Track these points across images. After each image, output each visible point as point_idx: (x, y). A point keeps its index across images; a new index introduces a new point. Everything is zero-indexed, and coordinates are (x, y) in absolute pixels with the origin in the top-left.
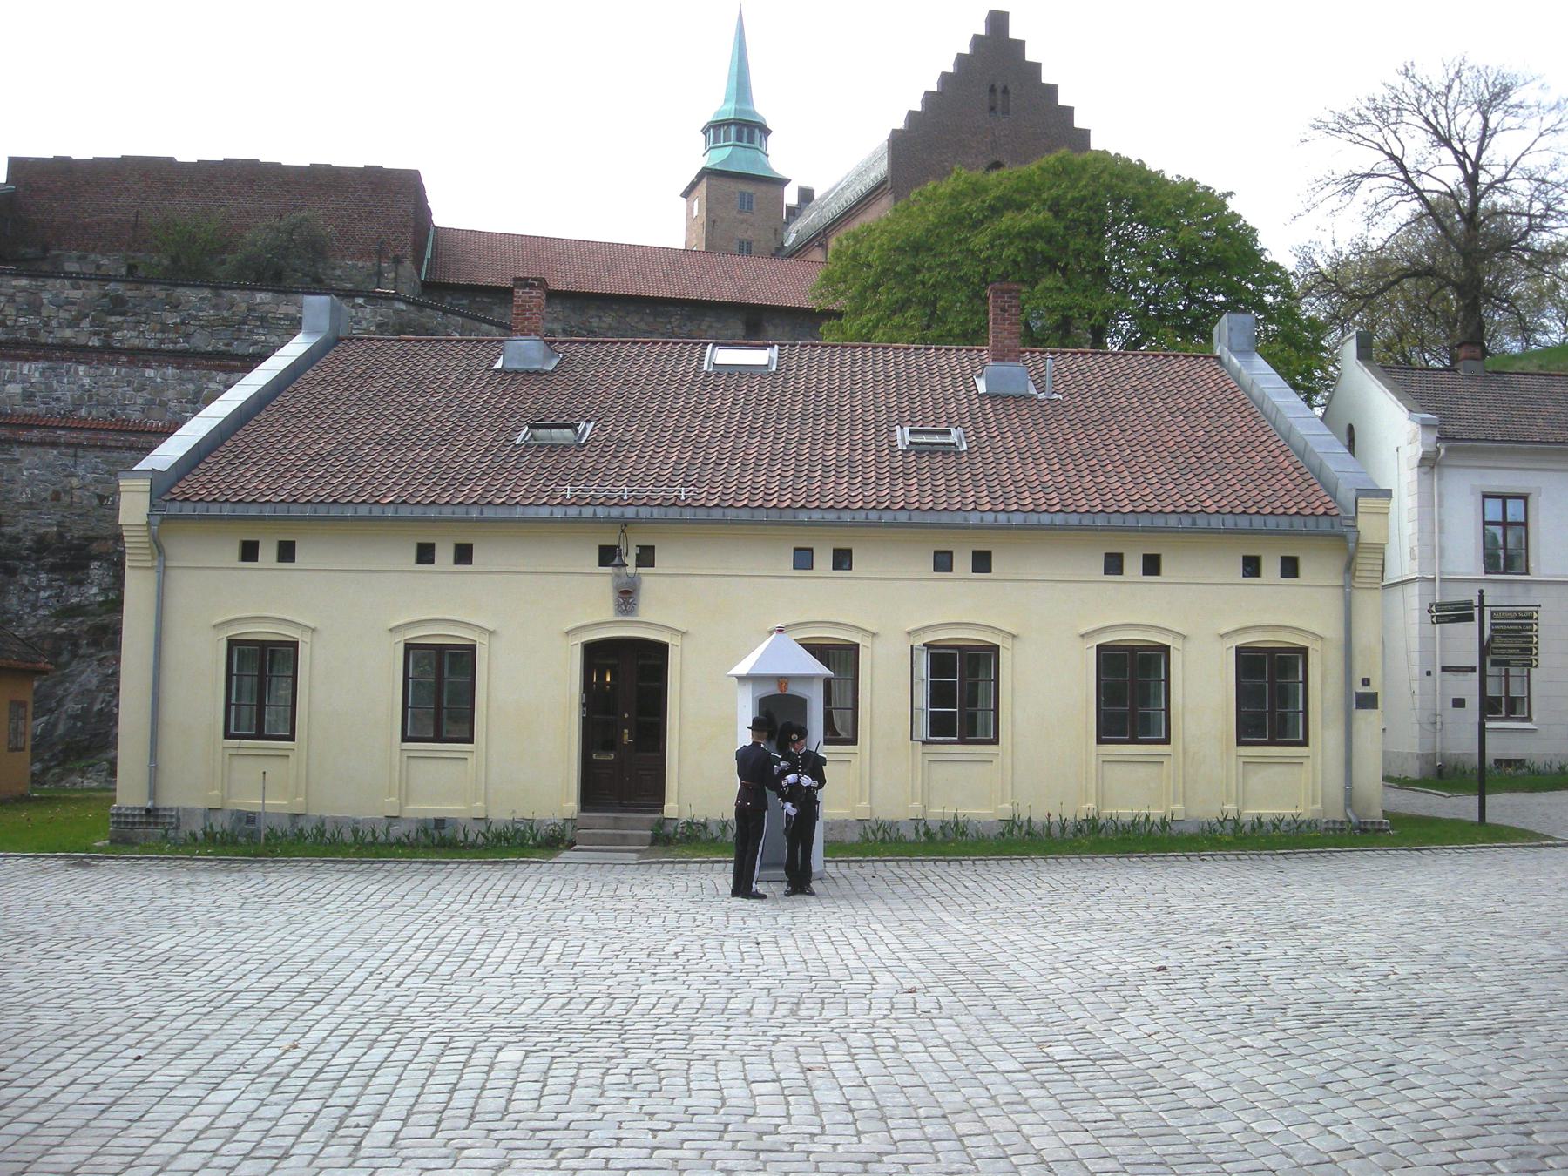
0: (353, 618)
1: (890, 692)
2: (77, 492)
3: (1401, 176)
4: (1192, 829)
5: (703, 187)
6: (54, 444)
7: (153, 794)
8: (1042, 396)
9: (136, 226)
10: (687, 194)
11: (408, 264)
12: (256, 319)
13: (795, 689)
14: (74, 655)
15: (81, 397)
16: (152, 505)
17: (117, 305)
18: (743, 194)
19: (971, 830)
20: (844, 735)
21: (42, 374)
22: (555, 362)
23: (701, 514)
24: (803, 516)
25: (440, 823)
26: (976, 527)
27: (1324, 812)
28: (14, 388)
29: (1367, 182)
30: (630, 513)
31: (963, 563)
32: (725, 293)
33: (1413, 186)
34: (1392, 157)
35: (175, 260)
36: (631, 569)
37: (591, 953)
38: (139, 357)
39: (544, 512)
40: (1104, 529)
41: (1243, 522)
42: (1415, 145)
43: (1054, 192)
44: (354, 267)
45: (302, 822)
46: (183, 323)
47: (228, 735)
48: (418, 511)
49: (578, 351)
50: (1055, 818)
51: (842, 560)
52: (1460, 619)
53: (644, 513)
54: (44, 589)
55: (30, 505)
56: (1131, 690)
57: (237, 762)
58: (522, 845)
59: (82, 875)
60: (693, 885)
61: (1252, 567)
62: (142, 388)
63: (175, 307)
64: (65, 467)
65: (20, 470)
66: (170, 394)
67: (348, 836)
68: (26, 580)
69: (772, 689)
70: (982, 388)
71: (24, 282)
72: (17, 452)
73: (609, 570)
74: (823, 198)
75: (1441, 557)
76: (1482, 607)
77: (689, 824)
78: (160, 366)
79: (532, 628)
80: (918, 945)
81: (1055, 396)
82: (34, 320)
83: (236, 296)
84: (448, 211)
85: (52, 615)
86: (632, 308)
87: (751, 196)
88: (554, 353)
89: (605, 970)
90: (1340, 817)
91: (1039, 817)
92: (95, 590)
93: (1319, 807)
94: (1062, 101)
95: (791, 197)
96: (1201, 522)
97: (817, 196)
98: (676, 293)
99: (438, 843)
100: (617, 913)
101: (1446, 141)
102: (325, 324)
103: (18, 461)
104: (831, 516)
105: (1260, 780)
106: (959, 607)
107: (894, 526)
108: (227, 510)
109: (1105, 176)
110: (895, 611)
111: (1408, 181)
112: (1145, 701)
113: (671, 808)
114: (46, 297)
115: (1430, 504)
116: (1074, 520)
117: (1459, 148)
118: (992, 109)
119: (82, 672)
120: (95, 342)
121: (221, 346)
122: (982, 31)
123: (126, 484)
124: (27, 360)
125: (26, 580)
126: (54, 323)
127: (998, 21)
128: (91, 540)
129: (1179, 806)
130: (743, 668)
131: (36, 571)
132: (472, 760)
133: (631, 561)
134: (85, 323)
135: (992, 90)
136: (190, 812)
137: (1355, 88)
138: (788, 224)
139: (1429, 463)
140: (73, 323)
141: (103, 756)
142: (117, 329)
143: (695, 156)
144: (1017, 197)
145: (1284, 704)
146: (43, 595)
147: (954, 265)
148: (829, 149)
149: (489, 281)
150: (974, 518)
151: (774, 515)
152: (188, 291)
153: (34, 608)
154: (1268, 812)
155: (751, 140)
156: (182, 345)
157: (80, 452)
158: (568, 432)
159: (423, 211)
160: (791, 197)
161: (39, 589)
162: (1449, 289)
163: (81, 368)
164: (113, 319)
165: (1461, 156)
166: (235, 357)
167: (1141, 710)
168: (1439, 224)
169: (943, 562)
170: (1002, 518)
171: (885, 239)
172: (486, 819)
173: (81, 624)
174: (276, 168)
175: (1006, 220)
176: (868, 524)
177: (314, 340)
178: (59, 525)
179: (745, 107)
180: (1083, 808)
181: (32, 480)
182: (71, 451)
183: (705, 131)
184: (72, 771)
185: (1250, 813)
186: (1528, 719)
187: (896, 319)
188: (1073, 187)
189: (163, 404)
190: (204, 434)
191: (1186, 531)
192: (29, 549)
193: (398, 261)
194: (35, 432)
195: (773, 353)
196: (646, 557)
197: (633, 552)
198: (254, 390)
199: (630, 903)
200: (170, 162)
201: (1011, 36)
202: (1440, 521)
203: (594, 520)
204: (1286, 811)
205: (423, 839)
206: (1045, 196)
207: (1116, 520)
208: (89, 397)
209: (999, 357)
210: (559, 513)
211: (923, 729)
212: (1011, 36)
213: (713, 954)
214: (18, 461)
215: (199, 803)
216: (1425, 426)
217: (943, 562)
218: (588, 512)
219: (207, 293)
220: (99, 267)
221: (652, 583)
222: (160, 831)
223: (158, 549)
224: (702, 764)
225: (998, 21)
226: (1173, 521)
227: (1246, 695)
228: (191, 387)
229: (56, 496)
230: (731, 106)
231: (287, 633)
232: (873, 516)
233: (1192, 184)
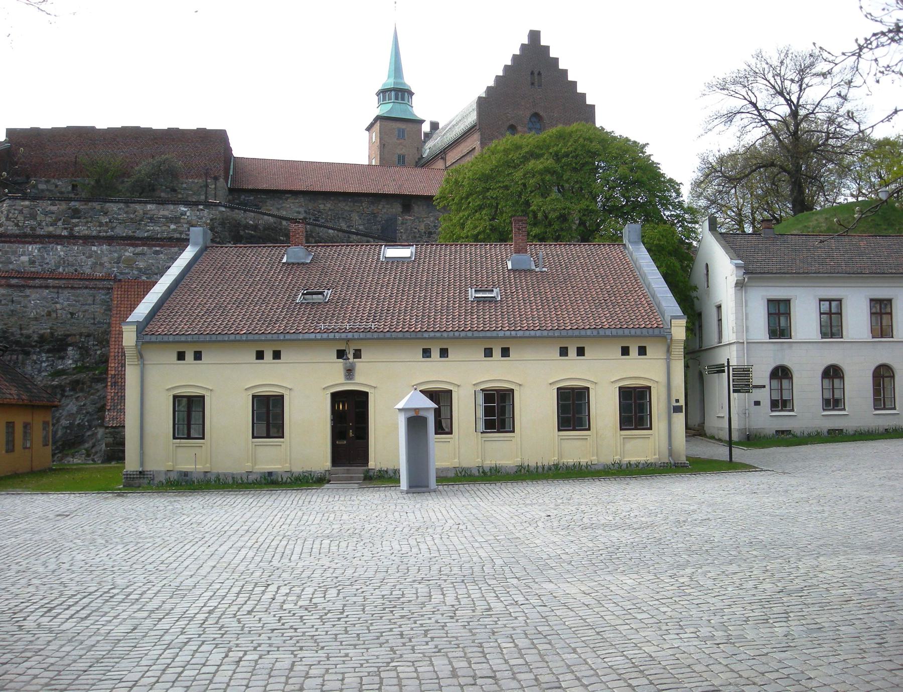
0: (229, 385)
1: (466, 411)
2: (60, 312)
3: (756, 112)
4: (601, 468)
5: (378, 124)
6: (47, 287)
7: (142, 464)
8: (537, 269)
9: (76, 163)
10: (369, 129)
11: (221, 180)
12: (148, 218)
13: (422, 414)
14: (63, 396)
15: (59, 262)
17: (76, 213)
18: (399, 130)
19: (503, 471)
20: (447, 430)
21: (39, 251)
22: (311, 257)
23: (381, 335)
24: (426, 335)
25: (270, 474)
26: (501, 338)
27: (659, 459)
28: (25, 259)
29: (738, 116)
30: (350, 335)
31: (497, 353)
32: (390, 189)
33: (762, 117)
34: (751, 102)
35: (98, 181)
36: (351, 360)
37: (345, 517)
38: (88, 240)
39: (312, 336)
40: (558, 337)
41: (620, 332)
42: (763, 97)
43: (555, 148)
44: (193, 182)
45: (209, 475)
46: (110, 221)
47: (174, 438)
48: (256, 337)
49: (321, 251)
50: (540, 464)
51: (444, 353)
52: (719, 372)
53: (356, 335)
54: (44, 362)
55: (36, 319)
56: (573, 408)
57: (180, 449)
58: (307, 482)
59: (119, 500)
60: (382, 495)
61: (625, 351)
62: (90, 257)
63: (106, 214)
64: (52, 299)
65: (30, 301)
66: (105, 259)
67: (231, 481)
68: (35, 357)
69: (412, 414)
70: (510, 267)
71: (27, 203)
73: (341, 360)
74: (444, 129)
75: (747, 332)
76: (728, 366)
77: (380, 471)
78: (100, 245)
79: (308, 387)
80: (466, 512)
81: (544, 269)
83: (138, 207)
84: (240, 149)
85: (49, 375)
86: (341, 198)
87: (403, 130)
88: (309, 253)
89: (352, 521)
90: (666, 461)
91: (533, 464)
93: (657, 456)
94: (570, 78)
95: (426, 128)
96: (602, 332)
97: (440, 127)
98: (364, 189)
99: (270, 482)
100: (353, 506)
101: (781, 94)
102: (201, 240)
103: (28, 296)
104: (438, 335)
105: (630, 445)
106: (497, 373)
107: (466, 337)
108: (171, 338)
109: (581, 140)
110: (467, 376)
111: (760, 115)
113: (372, 464)
115: (742, 304)
116: (545, 333)
117: (788, 97)
118: (533, 84)
119: (68, 405)
120: (65, 233)
121: (130, 233)
122: (526, 42)
123: (125, 328)
124: (30, 243)
125: (35, 357)
126: (44, 224)
127: (535, 36)
129: (595, 458)
130: (401, 405)
132: (283, 446)
133: (351, 356)
134: (60, 223)
135: (532, 73)
136: (159, 472)
137: (734, 63)
138: (425, 142)
139: (740, 285)
141: (82, 447)
142: (76, 226)
143: (373, 109)
144: (537, 151)
146: (44, 365)
147: (506, 188)
148: (448, 102)
149: (265, 186)
150: (501, 334)
151: (413, 335)
152: (112, 205)
153: (40, 371)
154: (634, 459)
155: (403, 99)
156: (110, 233)
157: (60, 291)
158: (320, 296)
159: (229, 150)
160: (426, 128)
161: (42, 362)
162: (791, 173)
163: (59, 247)
164: (74, 221)
165: (789, 102)
166: (138, 239)
168: (777, 137)
169: (488, 353)
170: (513, 333)
171: (471, 173)
172: (290, 472)
173: (64, 380)
174: (149, 131)
175: (531, 164)
176: (454, 338)
177: (197, 249)
178: (51, 328)
179: (399, 81)
180: (551, 459)
181: (36, 305)
182: (56, 290)
184: (67, 455)
185: (626, 460)
186: (793, 410)
187: (477, 215)
188: (565, 145)
189: (102, 264)
190: (155, 301)
191: (594, 337)
192: (36, 341)
193: (216, 179)
194: (37, 281)
195: (413, 249)
196: (358, 354)
197: (352, 352)
198: (173, 278)
199: (357, 502)
200: (93, 129)
201: (542, 44)
202: (746, 314)
203: (334, 339)
204: (642, 459)
205: (263, 481)
206: (551, 151)
207: (564, 333)
208: (63, 262)
209: (518, 251)
210: (319, 336)
211: (481, 426)
212: (542, 44)
213: (390, 516)
214: (28, 296)
215: (163, 469)
216: (738, 267)
217: (488, 353)
218: (331, 336)
219: (122, 205)
220: (56, 186)
221: (360, 366)
222: (146, 481)
223: (141, 356)
224: (388, 441)
225: (535, 36)
226: (589, 332)
228: (116, 255)
230: (392, 80)
231: (199, 392)
232: (457, 334)
233: (627, 140)
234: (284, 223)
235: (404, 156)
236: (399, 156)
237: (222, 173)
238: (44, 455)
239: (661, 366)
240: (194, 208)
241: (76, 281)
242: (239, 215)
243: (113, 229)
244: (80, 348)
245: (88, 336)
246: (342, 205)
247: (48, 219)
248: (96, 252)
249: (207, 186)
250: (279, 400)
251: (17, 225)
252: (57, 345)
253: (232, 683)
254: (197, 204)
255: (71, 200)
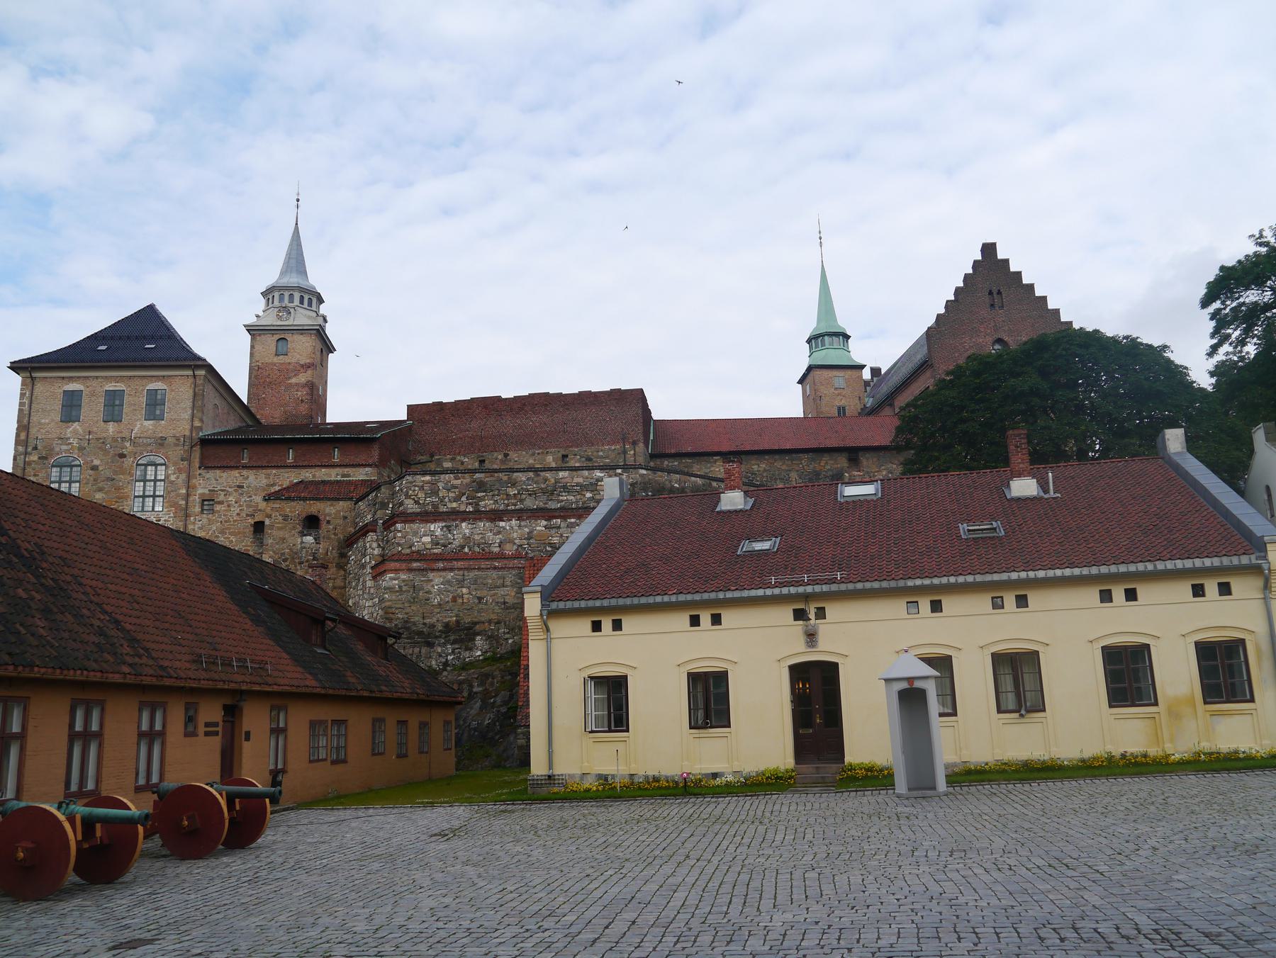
1: (974, 681)
6: (451, 570)
7: (551, 767)
10: (801, 382)
13: (918, 684)
16: (543, 605)
17: (481, 486)
28: (427, 539)
38: (495, 516)
45: (636, 780)
56: (1127, 674)
62: (499, 533)
63: (514, 485)
66: (515, 535)
68: (439, 650)
69: (905, 685)
71: (428, 478)
72: (431, 575)
73: (801, 622)
82: (435, 499)
92: (479, 653)
106: (1012, 627)
112: (1137, 680)
114: (441, 485)
120: (470, 509)
125: (439, 650)
127: (989, 249)
128: (476, 623)
131: (444, 644)
133: (812, 616)
134: (464, 499)
135: (991, 293)
140: (457, 499)
145: (1232, 676)
152: (520, 474)
163: (464, 524)
167: (1135, 685)
183: (809, 341)
193: (634, 443)
198: (585, 535)
208: (467, 539)
220: (462, 463)
224: (869, 733)
225: (989, 249)
227: (1206, 672)
229: (454, 599)
234: (714, 484)
235: (844, 408)
236: (839, 409)
237: (641, 437)
238: (447, 761)
239: (1256, 607)
240: (611, 472)
241: (484, 557)
242: (662, 477)
243: (521, 501)
244: (489, 637)
245: (498, 622)
246: (778, 464)
247: (451, 495)
248: (504, 528)
249: (625, 452)
250: (720, 678)
251: (417, 502)
252: (462, 633)
253: (725, 909)
254: (614, 468)
255: (474, 471)
